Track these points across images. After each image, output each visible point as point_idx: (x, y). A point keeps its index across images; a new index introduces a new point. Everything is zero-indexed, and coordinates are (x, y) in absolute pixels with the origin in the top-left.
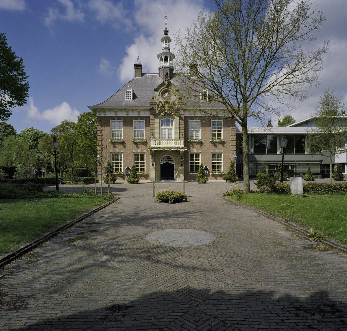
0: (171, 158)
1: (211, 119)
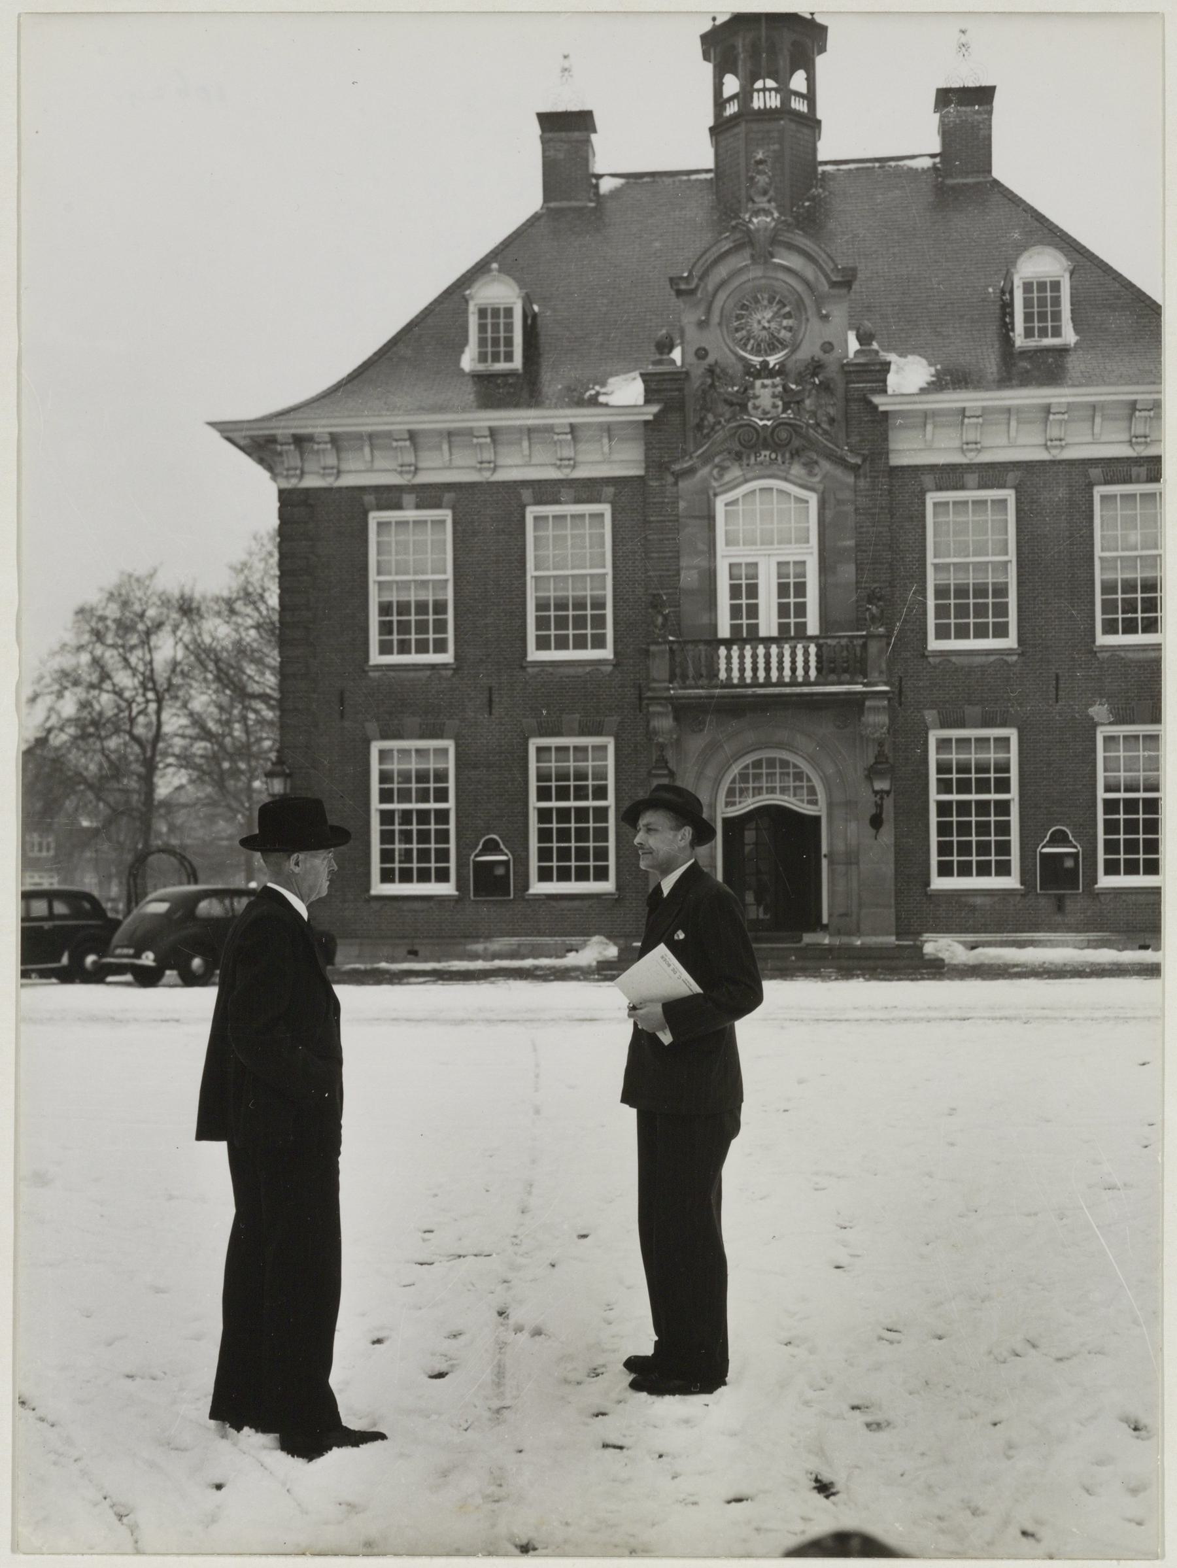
0: (799, 776)
1: (928, 480)
